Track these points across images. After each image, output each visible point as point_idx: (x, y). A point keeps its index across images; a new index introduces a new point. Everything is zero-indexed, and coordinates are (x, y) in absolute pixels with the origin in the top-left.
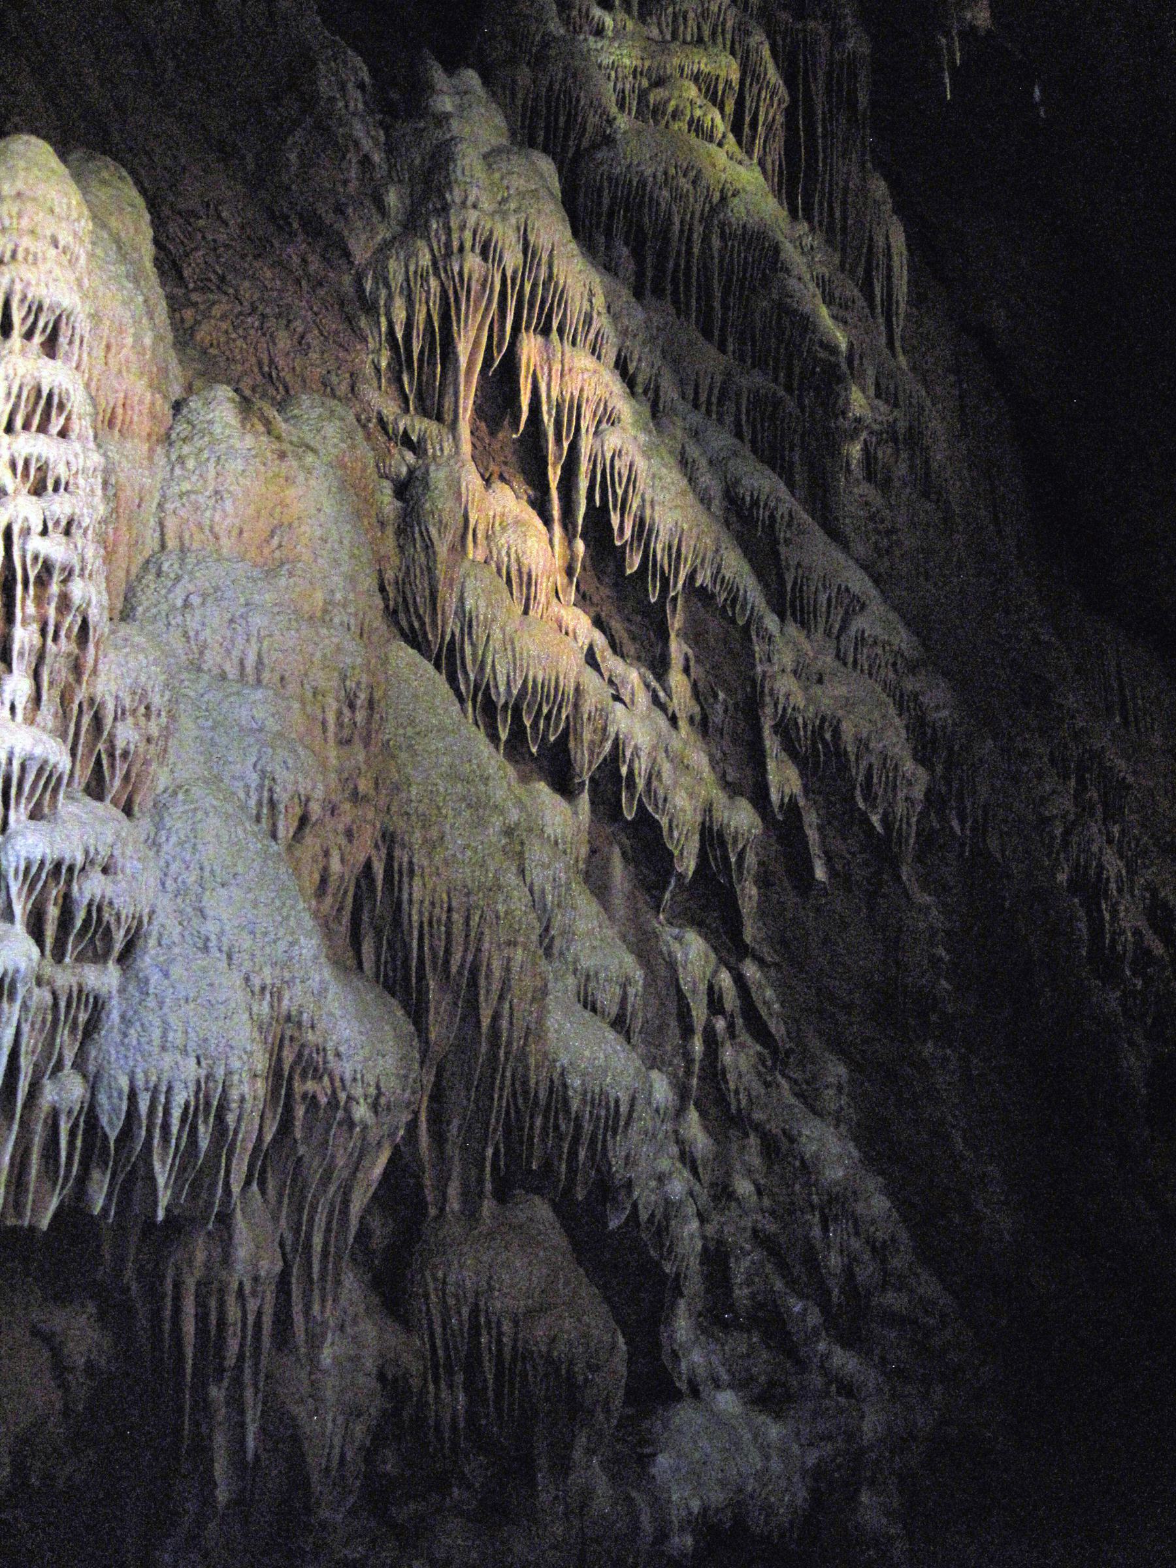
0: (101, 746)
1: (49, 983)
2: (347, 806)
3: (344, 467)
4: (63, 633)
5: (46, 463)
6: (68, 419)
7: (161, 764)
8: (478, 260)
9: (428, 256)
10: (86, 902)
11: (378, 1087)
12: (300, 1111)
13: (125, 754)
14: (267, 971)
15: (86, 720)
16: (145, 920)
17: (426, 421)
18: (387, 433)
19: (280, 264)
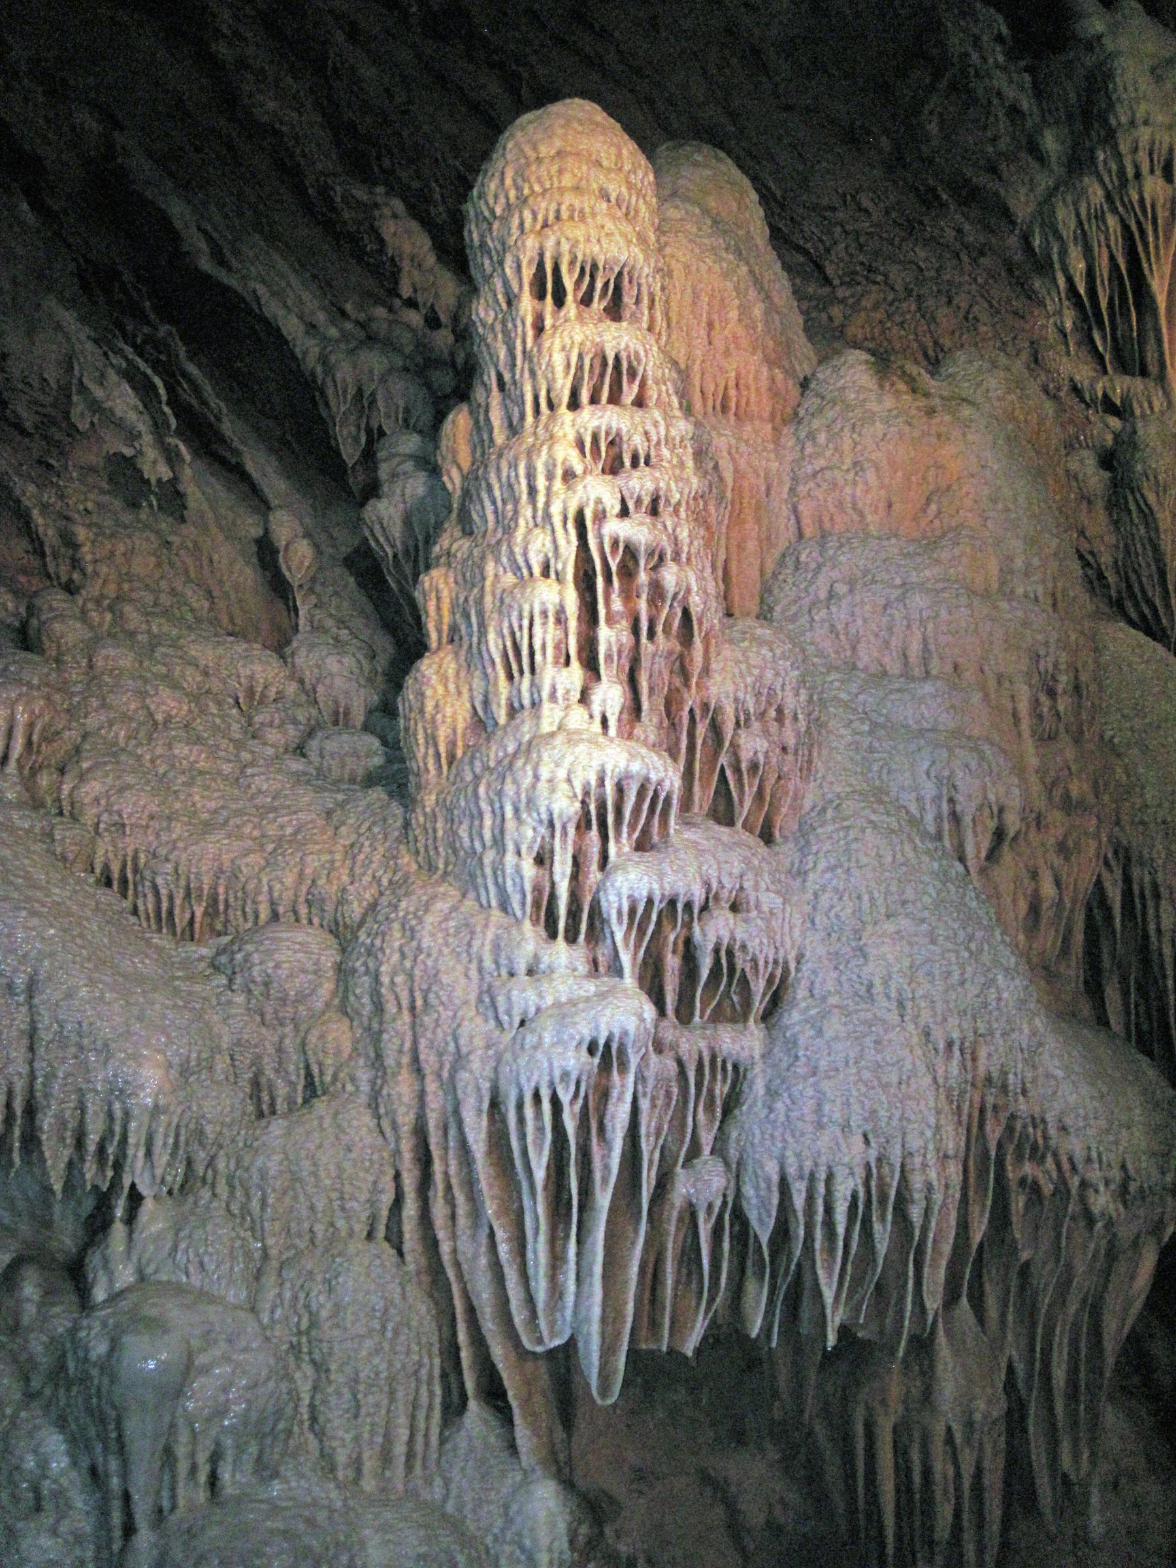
0: (723, 760)
1: (672, 1048)
2: (1057, 816)
3: (1012, 418)
4: (659, 629)
5: (618, 435)
6: (643, 385)
7: (805, 779)
8: (1161, 182)
9: (1100, 192)
10: (711, 946)
11: (1123, 1167)
12: (1018, 1202)
13: (754, 767)
14: (953, 1021)
15: (701, 730)
16: (792, 966)
17: (1128, 378)
18: (1082, 400)
19: (932, 242)
